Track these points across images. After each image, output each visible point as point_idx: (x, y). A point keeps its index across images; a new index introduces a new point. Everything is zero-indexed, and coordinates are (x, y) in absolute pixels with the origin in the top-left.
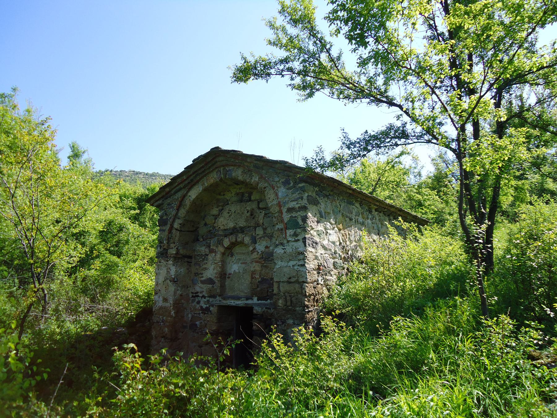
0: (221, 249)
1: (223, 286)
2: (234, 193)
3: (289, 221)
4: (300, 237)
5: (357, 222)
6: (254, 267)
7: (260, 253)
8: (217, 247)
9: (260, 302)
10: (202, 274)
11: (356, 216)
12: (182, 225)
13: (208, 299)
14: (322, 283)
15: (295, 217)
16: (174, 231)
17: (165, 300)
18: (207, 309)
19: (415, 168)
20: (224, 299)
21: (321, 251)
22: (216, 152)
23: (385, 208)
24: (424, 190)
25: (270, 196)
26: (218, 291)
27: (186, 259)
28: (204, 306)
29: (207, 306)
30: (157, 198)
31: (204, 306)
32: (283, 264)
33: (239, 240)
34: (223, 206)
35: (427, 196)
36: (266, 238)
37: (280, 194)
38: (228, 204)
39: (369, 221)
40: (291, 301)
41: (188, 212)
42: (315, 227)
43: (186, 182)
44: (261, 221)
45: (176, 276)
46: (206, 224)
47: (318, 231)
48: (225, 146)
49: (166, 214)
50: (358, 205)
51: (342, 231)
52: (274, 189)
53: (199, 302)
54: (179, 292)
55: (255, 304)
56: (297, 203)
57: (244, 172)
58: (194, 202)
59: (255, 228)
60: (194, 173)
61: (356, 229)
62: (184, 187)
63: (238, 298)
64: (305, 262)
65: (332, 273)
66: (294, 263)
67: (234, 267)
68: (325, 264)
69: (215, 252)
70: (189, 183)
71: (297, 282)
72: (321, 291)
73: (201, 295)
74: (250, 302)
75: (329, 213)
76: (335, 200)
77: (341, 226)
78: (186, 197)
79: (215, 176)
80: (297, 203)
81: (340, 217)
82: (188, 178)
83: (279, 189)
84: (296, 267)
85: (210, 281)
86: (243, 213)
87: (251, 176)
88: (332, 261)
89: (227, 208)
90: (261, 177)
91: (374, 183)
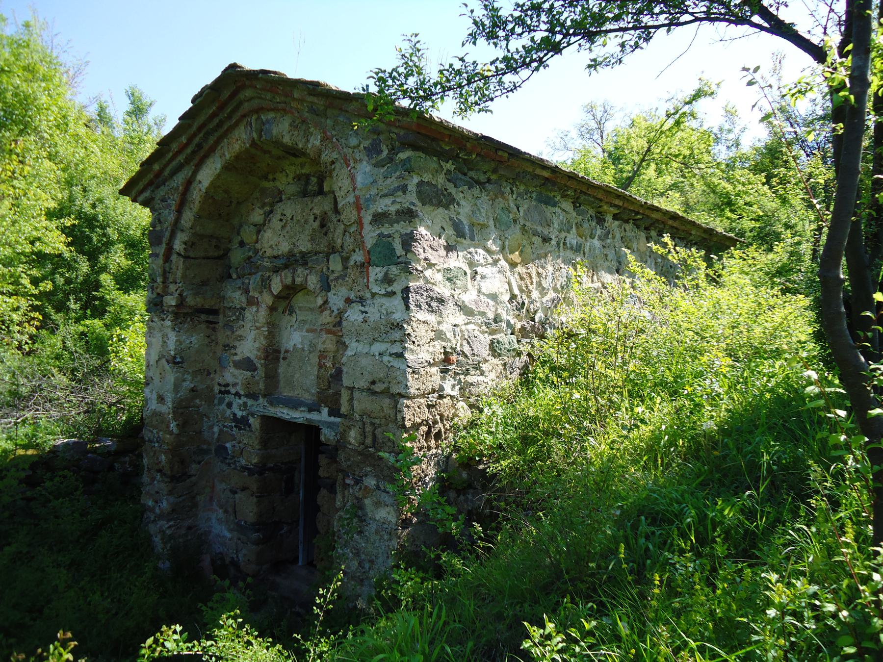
0: (267, 299)
1: (272, 377)
2: (291, 176)
3: (376, 245)
4: (397, 287)
5: (562, 244)
6: (324, 343)
7: (336, 312)
8: (261, 293)
9: (332, 419)
10: (235, 347)
11: (560, 231)
12: (190, 245)
13: (245, 399)
14: (455, 393)
15: (389, 236)
16: (174, 257)
17: (161, 399)
19: (730, 131)
20: (271, 404)
21: (452, 317)
22: (233, 76)
23: (637, 213)
24: (738, 173)
25: (340, 183)
26: (262, 386)
27: (203, 317)
29: (244, 413)
30: (141, 185)
31: (239, 414)
32: (362, 348)
33: (298, 280)
34: (272, 205)
35: (744, 185)
37: (359, 179)
38: (281, 200)
39: (596, 242)
40: (374, 436)
41: (198, 217)
42: (435, 257)
43: (189, 150)
44: (339, 241)
45: (180, 351)
46: (242, 244)
47: (449, 270)
48: (251, 63)
49: (160, 222)
50: (567, 205)
51: (520, 269)
52: (348, 166)
53: (230, 405)
54: (188, 384)
55: (325, 423)
56: (394, 202)
57: (294, 126)
58: (208, 196)
60: (200, 129)
61: (559, 261)
62: (187, 161)
63: (294, 404)
64: (405, 348)
65: (485, 367)
67: (294, 338)
68: (466, 349)
69: (258, 304)
70: (194, 152)
71: (386, 392)
72: (448, 413)
73: (233, 391)
74: (314, 416)
75: (483, 226)
76: (502, 194)
77: (516, 257)
78: (194, 185)
79: (244, 136)
80: (394, 202)
81: (515, 235)
82: (190, 141)
83: (358, 166)
84: (386, 358)
85: (247, 364)
86: (306, 222)
87: (307, 135)
88: (487, 339)
89: (279, 208)
90: (325, 139)
91: (637, 159)
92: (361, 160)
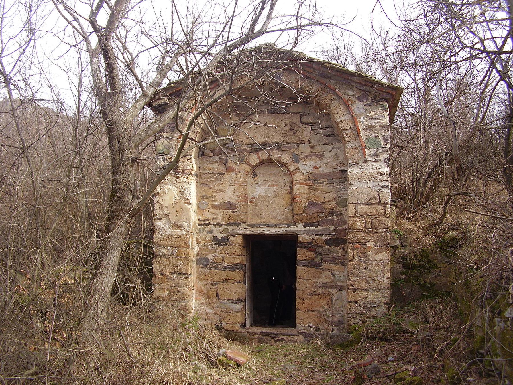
9: (307, 228)
13: (226, 227)
18: (225, 240)
28: (220, 236)
29: (225, 235)
53: (211, 232)
55: (300, 231)
56: (378, 122)
59: (298, 145)
63: (275, 226)
66: (376, 184)
80: (378, 122)
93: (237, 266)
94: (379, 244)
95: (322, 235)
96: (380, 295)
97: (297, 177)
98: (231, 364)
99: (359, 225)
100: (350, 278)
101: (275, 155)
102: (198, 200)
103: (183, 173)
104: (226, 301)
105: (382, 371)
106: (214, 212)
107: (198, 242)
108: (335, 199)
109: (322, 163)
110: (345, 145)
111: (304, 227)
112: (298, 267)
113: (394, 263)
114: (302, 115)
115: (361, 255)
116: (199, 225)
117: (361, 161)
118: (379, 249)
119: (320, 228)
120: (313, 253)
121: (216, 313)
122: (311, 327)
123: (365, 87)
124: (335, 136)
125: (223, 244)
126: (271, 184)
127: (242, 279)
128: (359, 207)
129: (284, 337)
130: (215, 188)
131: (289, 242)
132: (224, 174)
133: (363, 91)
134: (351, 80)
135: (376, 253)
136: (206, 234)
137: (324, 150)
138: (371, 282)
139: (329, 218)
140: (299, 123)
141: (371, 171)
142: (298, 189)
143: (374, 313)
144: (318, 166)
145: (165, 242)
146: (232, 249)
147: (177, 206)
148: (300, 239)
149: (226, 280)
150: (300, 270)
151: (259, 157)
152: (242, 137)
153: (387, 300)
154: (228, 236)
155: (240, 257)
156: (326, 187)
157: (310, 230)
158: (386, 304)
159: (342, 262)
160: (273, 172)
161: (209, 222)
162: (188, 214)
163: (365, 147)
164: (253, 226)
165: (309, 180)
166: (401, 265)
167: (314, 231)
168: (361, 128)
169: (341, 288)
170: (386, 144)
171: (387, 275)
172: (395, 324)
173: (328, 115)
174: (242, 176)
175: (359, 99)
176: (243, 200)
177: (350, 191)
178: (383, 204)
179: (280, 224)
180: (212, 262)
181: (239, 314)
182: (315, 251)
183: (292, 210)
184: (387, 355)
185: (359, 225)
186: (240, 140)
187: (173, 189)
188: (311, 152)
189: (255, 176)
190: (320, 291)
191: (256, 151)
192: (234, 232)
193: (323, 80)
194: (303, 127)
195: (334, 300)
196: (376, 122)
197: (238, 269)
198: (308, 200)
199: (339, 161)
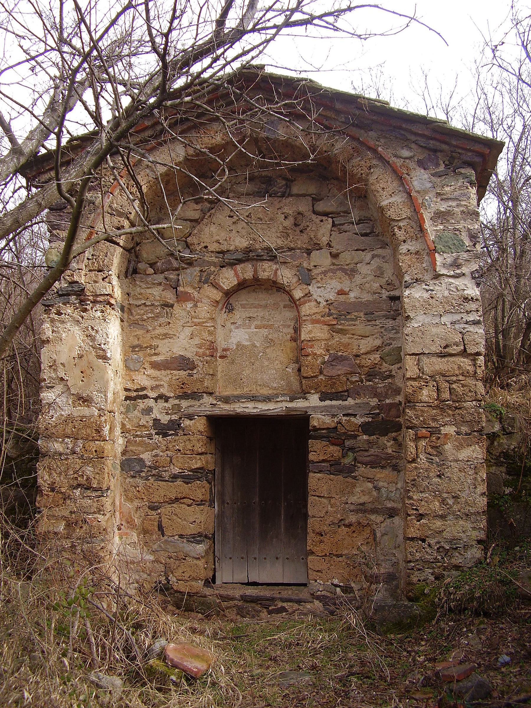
9: (328, 403)
13: (177, 402)
28: (165, 419)
29: (174, 417)
36: (339, 273)
53: (148, 411)
55: (314, 408)
63: (268, 399)
66: (457, 317)
92: (415, 169)
93: (198, 474)
94: (464, 429)
95: (355, 416)
96: (468, 525)
97: (307, 309)
98: (174, 678)
99: (427, 394)
100: (411, 494)
101: (266, 271)
102: (125, 353)
103: (95, 302)
104: (176, 537)
105: (495, 694)
106: (154, 375)
107: (124, 431)
108: (377, 349)
109: (354, 285)
110: (395, 249)
111: (321, 400)
112: (311, 475)
113: (491, 466)
114: (316, 200)
115: (430, 450)
116: (127, 398)
117: (427, 277)
118: (465, 440)
119: (350, 401)
120: (339, 448)
121: (157, 561)
122: (336, 586)
123: (431, 142)
124: (377, 235)
125: (171, 432)
126: (259, 323)
127: (208, 497)
128: (425, 360)
129: (285, 604)
130: (157, 332)
131: (296, 426)
132: (172, 306)
133: (430, 149)
134: (406, 130)
135: (459, 447)
136: (139, 415)
137: (356, 261)
138: (451, 502)
139: (368, 383)
140: (310, 213)
141: (446, 293)
142: (310, 332)
143: (457, 560)
144: (346, 289)
145: (60, 428)
146: (187, 443)
147: (84, 363)
148: (314, 423)
149: (177, 500)
150: (314, 480)
151: (236, 275)
152: (206, 240)
153: (482, 535)
154: (180, 418)
155: (202, 457)
156: (360, 327)
157: (332, 406)
158: (479, 542)
159: (394, 463)
160: (263, 303)
161: (145, 392)
162: (102, 378)
163: (435, 250)
164: (226, 400)
165: (330, 315)
166: (503, 469)
167: (339, 407)
168: (427, 216)
169: (392, 513)
170: (474, 245)
171: (482, 488)
172: (501, 581)
173: (363, 196)
174: (204, 309)
175: (421, 164)
176: (208, 352)
177: (407, 331)
178: (471, 354)
179: (277, 396)
180: (150, 467)
181: (201, 563)
182: (341, 444)
183: (299, 370)
184: (493, 649)
185: (427, 394)
186: (203, 245)
187: (77, 331)
188: (333, 264)
189: (230, 310)
190: (353, 518)
191: (232, 264)
192: (191, 410)
193: (355, 131)
194: (318, 221)
195: (378, 535)
196: (454, 204)
197: (198, 479)
198: (328, 350)
199: (384, 280)
